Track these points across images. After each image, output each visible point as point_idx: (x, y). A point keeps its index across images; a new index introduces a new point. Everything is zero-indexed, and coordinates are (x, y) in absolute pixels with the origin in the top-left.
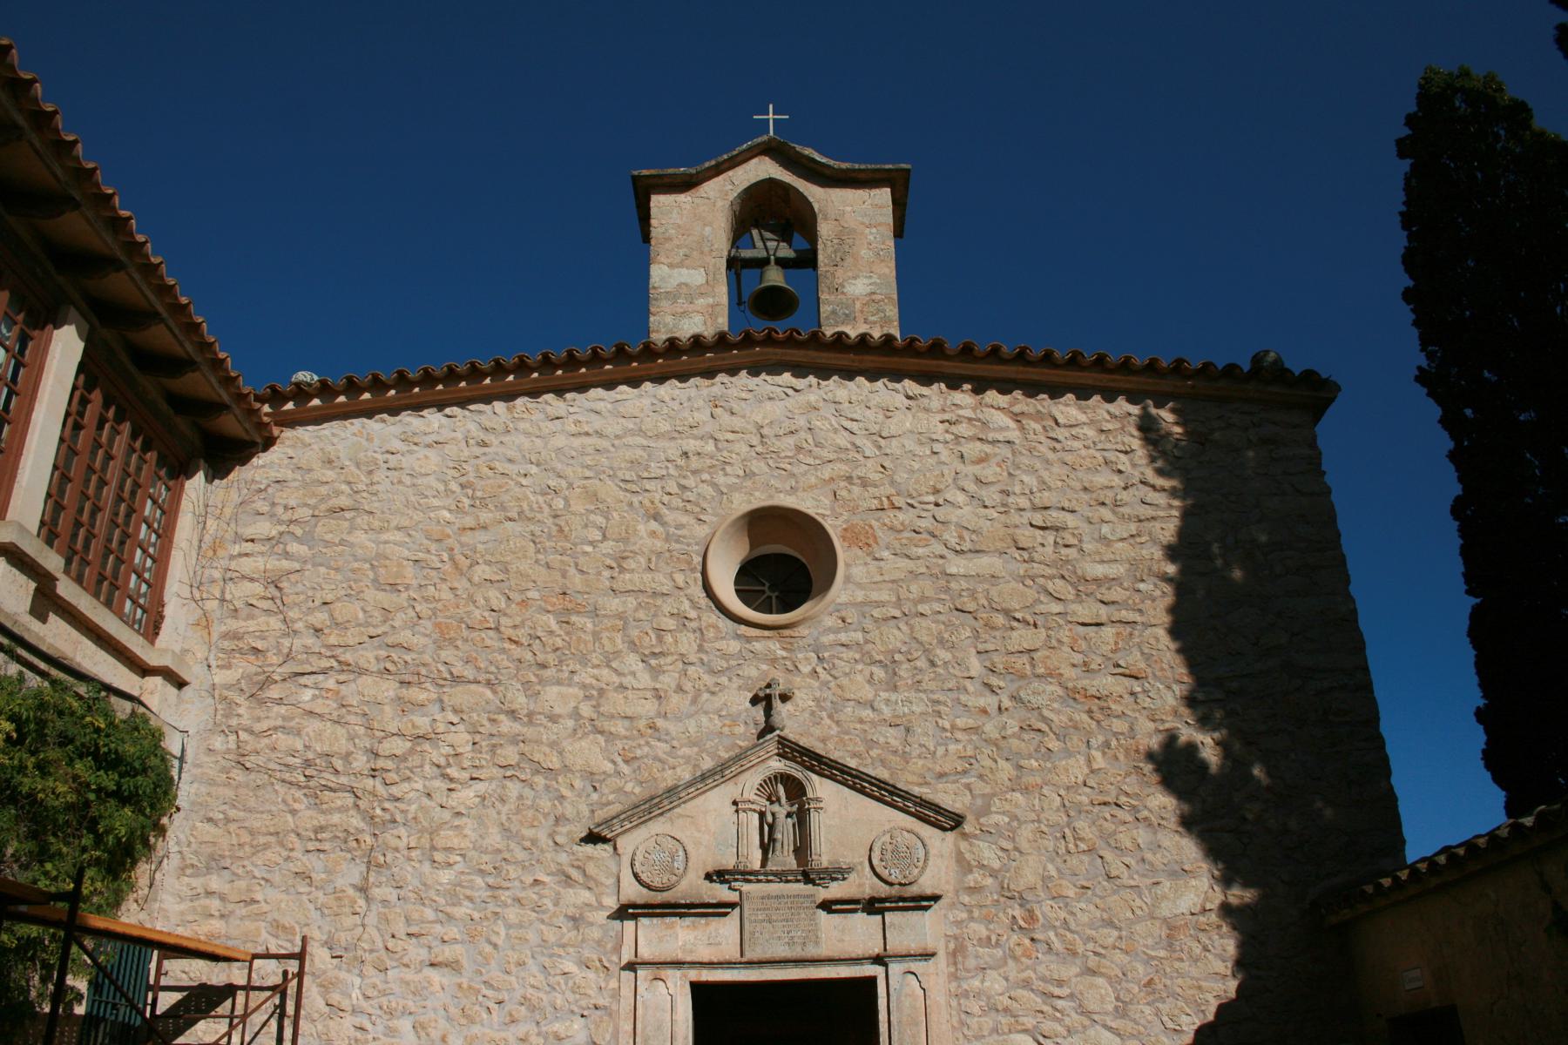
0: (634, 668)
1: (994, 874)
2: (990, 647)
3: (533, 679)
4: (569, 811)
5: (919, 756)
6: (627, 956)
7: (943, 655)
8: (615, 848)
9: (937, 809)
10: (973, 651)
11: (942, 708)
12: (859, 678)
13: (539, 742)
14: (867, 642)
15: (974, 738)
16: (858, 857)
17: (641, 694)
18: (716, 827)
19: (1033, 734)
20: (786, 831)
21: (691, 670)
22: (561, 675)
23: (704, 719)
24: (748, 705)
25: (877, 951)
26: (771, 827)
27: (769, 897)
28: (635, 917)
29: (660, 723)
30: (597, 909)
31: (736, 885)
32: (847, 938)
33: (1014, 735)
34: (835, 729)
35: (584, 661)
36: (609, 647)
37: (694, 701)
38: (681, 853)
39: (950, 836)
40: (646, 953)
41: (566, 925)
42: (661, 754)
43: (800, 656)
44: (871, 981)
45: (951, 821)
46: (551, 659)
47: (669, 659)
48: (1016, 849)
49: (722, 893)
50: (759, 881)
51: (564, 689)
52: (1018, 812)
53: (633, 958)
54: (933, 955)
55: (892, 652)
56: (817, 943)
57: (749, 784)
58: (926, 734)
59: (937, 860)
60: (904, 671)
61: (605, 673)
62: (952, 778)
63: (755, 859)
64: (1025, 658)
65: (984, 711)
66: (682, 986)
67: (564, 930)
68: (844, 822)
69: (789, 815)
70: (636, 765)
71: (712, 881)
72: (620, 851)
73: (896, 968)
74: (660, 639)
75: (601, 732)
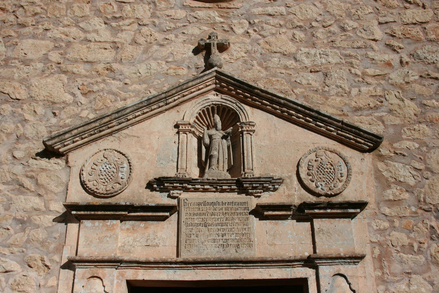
0: (98, 27)
1: (409, 189)
2: (389, 19)
3: (13, 34)
4: (29, 131)
5: (337, 94)
6: (68, 253)
7: (351, 24)
8: (67, 162)
9: (357, 131)
10: (376, 23)
11: (354, 61)
12: (283, 36)
13: (10, 79)
14: (289, 13)
15: (383, 82)
16: (286, 171)
17: (102, 45)
18: (159, 146)
19: (431, 81)
20: (221, 148)
21: (144, 30)
22: (36, 31)
23: (154, 64)
24: (191, 54)
25: (307, 254)
26: (208, 148)
27: (205, 203)
28: (79, 219)
29: (115, 66)
30: (44, 212)
31: (175, 193)
32: (278, 243)
33: (415, 81)
34: (264, 73)
35: (57, 22)
36: (78, 13)
37: (146, 51)
38: (126, 165)
39: (368, 157)
40: (85, 252)
41: (14, 228)
42: (114, 89)
43: (235, 21)
44: (304, 281)
45: (369, 143)
46: (30, 20)
47: (127, 22)
48: (428, 169)
49: (162, 199)
50: (196, 190)
51: (37, 42)
52: (425, 139)
53: (73, 255)
54: (362, 257)
55: (310, 21)
56: (250, 246)
57: (190, 112)
58: (342, 78)
59: (358, 177)
60: (320, 33)
61: (74, 31)
62: (365, 112)
63: (195, 173)
64: (418, 28)
65: (389, 64)
66: (119, 285)
67: (12, 231)
68: (271, 144)
69: (224, 137)
70: (92, 96)
71: (153, 189)
72: (71, 163)
73: (326, 271)
74: (121, 9)
75: (65, 72)
